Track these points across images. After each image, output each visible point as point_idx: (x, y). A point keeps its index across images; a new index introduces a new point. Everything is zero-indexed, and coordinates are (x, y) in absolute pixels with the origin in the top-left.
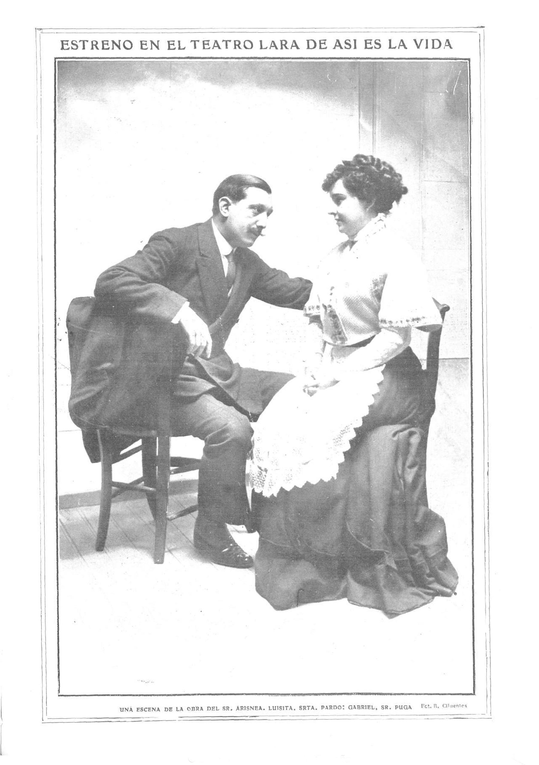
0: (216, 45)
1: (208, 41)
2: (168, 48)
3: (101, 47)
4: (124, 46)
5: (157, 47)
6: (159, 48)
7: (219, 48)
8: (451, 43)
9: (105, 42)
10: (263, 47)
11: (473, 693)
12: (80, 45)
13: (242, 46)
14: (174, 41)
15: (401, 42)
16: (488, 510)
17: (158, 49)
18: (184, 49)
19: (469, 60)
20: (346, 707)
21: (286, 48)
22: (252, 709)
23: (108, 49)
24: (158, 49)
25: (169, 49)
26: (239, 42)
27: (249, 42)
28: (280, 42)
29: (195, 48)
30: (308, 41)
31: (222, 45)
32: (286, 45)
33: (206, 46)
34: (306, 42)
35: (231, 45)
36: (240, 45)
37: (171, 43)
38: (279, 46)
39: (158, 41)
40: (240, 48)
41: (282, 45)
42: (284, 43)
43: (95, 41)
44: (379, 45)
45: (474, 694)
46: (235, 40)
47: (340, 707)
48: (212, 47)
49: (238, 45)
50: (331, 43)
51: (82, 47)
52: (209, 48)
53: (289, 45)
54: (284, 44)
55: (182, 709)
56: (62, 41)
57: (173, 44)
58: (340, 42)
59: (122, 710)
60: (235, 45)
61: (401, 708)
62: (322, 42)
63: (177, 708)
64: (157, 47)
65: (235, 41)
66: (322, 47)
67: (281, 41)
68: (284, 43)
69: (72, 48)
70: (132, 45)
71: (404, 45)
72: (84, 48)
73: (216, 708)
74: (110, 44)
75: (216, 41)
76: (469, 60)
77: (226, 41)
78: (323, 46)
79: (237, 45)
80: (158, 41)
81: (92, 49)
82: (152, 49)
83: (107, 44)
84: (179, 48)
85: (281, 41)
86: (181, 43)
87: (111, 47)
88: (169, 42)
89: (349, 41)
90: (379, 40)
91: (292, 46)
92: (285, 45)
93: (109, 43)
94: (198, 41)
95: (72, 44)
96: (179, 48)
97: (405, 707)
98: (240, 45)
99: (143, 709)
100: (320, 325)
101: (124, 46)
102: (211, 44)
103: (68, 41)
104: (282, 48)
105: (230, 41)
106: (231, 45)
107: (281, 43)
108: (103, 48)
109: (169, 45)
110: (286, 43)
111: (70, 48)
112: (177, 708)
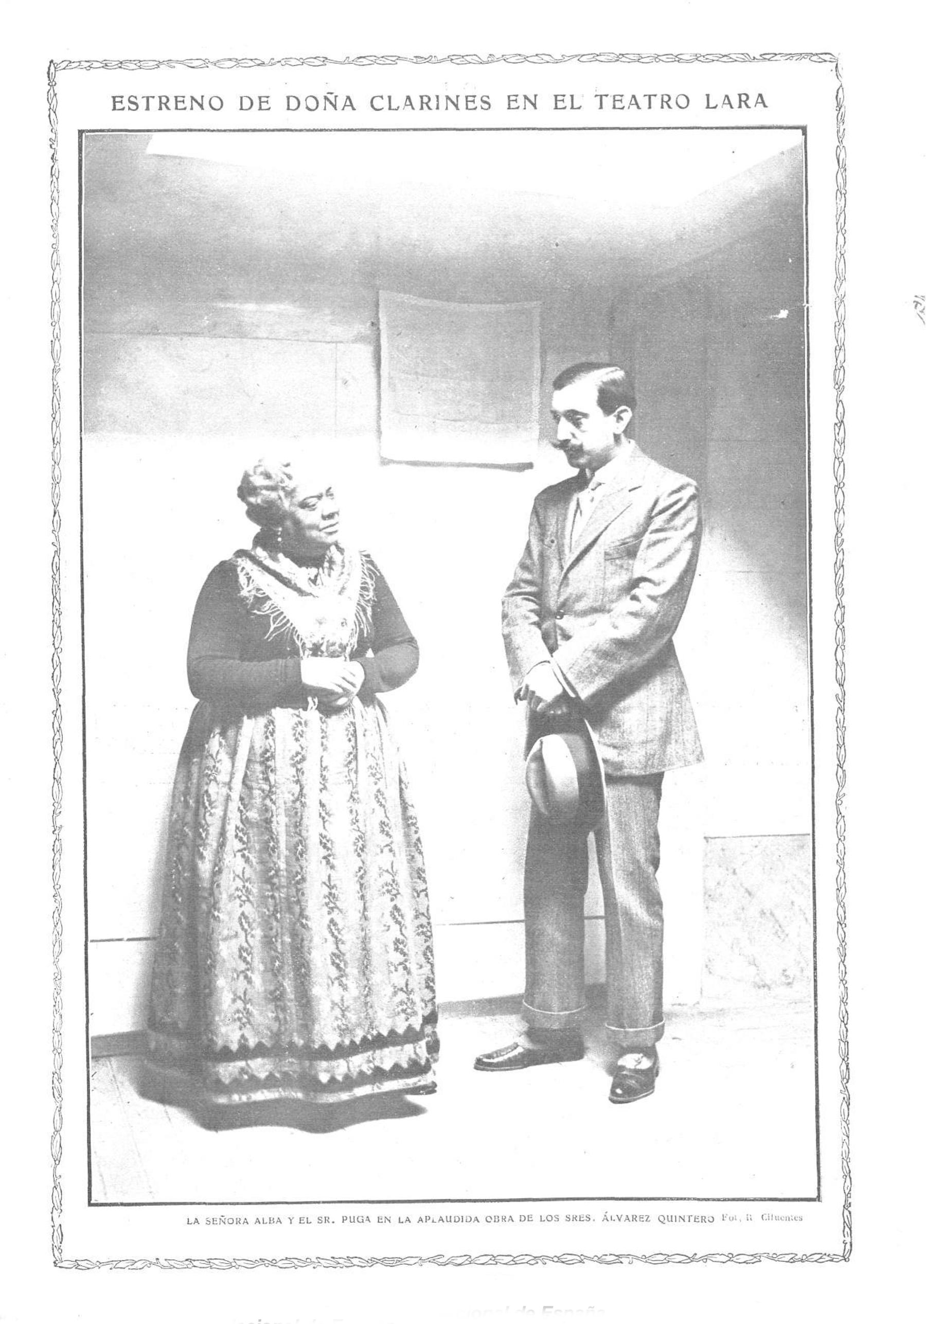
1: (622, 96)
2: (554, 106)
3: (174, 106)
5: (534, 105)
8: (765, 99)
10: (711, 106)
11: (92, 1202)
12: (142, 103)
13: (672, 103)
15: (348, 101)
17: (203, 109)
18: (579, 108)
19: (81, 132)
20: (536, 1218)
21: (747, 106)
22: (222, 1223)
24: (536, 108)
25: (556, 108)
28: (738, 97)
29: (601, 107)
30: (288, 98)
31: (643, 102)
32: (669, 103)
33: (618, 104)
34: (286, 99)
38: (631, 1219)
39: (535, 96)
40: (168, 108)
42: (744, 97)
43: (166, 97)
44: (487, 103)
45: (90, 1204)
46: (288, 94)
47: (549, 1218)
50: (277, 102)
51: (145, 107)
54: (743, 100)
55: (197, 1221)
57: (473, 101)
59: (670, 1219)
61: (352, 1220)
62: (263, 102)
63: (708, 96)
64: (534, 105)
67: (740, 95)
68: (425, 100)
69: (129, 109)
71: (763, 102)
72: (148, 109)
73: (305, 1220)
74: (521, 100)
75: (634, 97)
76: (81, 132)
77: (601, 96)
78: (264, 106)
79: (666, 102)
80: (535, 96)
81: (161, 109)
82: (192, 109)
84: (572, 108)
86: (574, 97)
88: (114, 98)
89: (136, 97)
90: (488, 97)
91: (757, 103)
93: (185, 99)
94: (655, 95)
95: (130, 102)
96: (572, 108)
97: (360, 1220)
99: (554, 1219)
102: (627, 100)
103: (122, 97)
104: (422, 108)
105: (607, 96)
106: (656, 102)
108: (176, 108)
109: (114, 102)
110: (748, 98)
111: (127, 108)
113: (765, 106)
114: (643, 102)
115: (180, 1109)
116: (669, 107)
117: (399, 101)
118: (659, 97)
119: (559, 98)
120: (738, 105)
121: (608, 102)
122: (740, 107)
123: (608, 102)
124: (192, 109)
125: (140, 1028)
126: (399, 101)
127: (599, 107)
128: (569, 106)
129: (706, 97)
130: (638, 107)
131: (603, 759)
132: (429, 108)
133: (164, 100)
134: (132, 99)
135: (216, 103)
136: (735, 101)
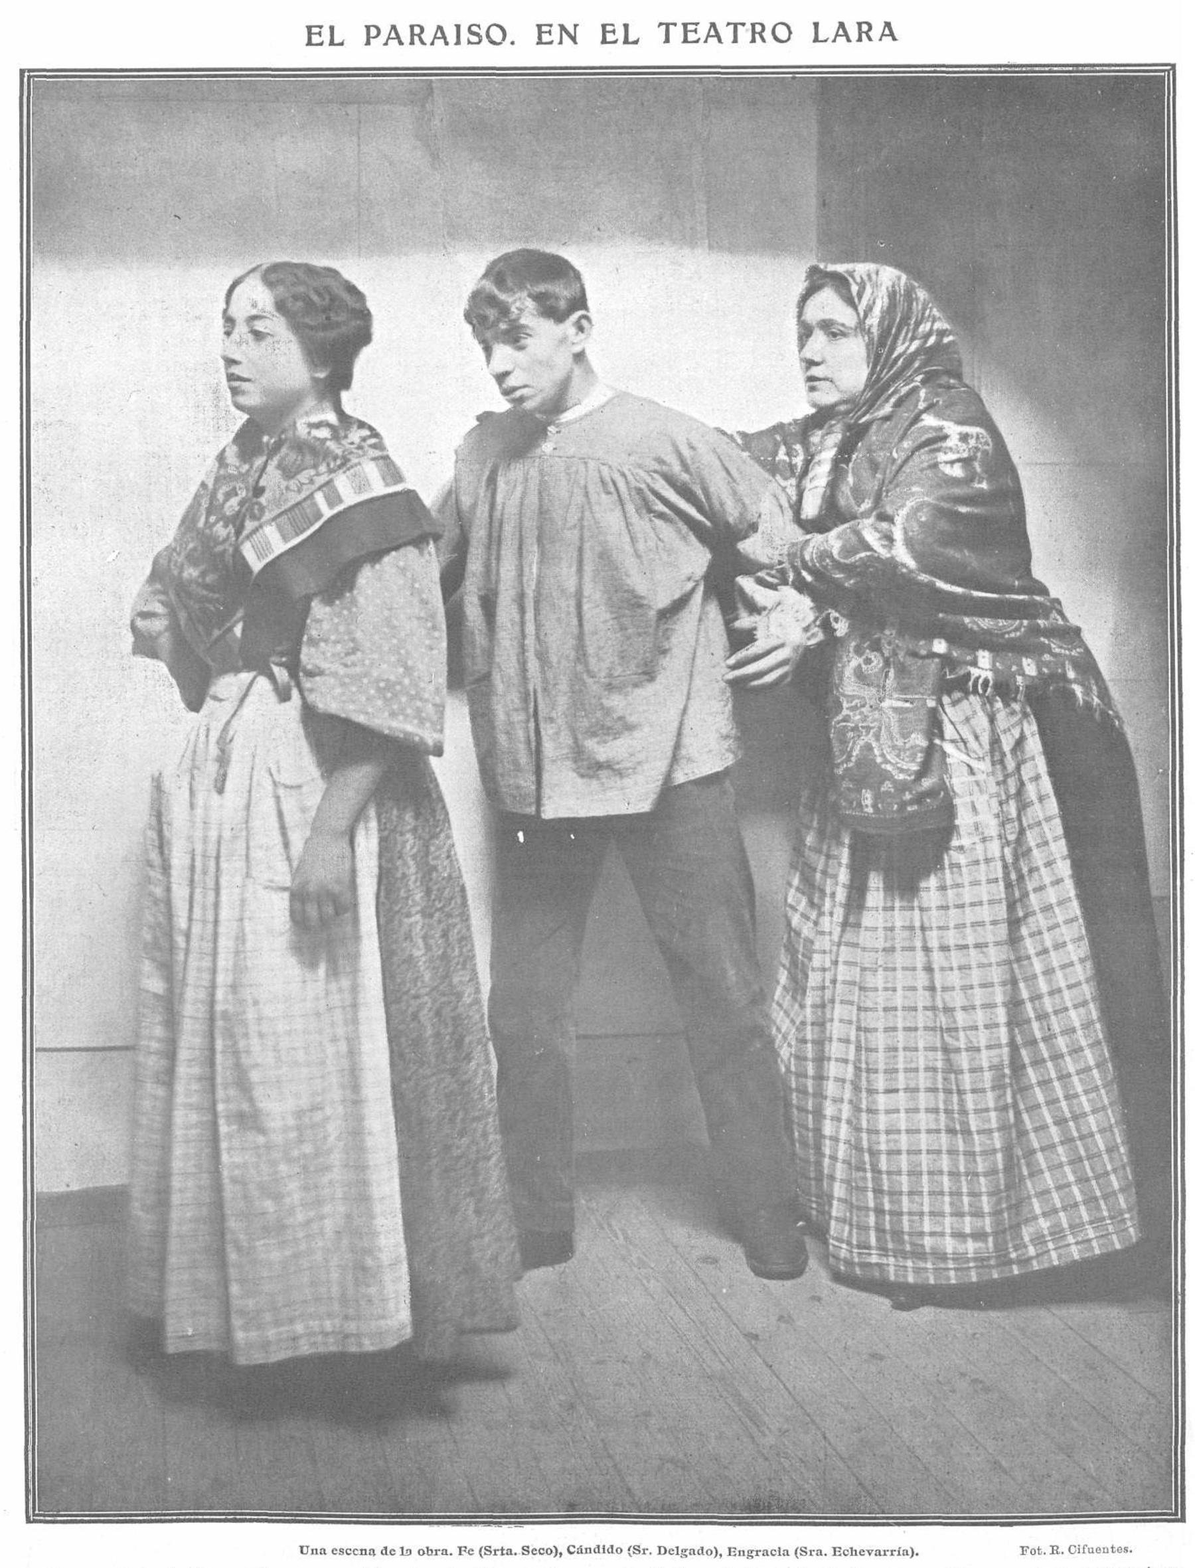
0: (712, 33)
1: (697, 24)
2: (306, 41)
4: (488, 36)
5: (574, 39)
6: (578, 40)
7: (720, 41)
9: (544, 29)
13: (767, 34)
14: (551, 26)
16: (853, 1552)
17: (575, 43)
19: (22, 72)
23: (551, 43)
24: (575, 43)
26: (763, 26)
27: (498, 30)
29: (667, 40)
31: (726, 33)
35: (744, 34)
36: (870, 33)
37: (544, 29)
38: (853, 34)
39: (576, 26)
41: (412, 34)
46: (860, 20)
48: (703, 39)
49: (760, 34)
52: (697, 41)
53: (428, 36)
56: (539, 26)
58: (445, 30)
60: (754, 32)
63: (816, 25)
64: (574, 39)
65: (753, 25)
66: (690, 39)
67: (412, 27)
70: (790, 33)
71: (892, 34)
73: (326, 33)
74: (556, 30)
75: (713, 25)
77: (736, 25)
79: (757, 32)
80: (576, 26)
81: (753, 41)
82: (561, 43)
83: (614, 32)
84: (332, 43)
85: (860, 24)
87: (557, 40)
91: (883, 35)
92: (867, 33)
98: (870, 33)
100: (489, 761)
101: (488, 36)
102: (703, 30)
103: (321, 27)
104: (412, 43)
106: (744, 34)
107: (860, 29)
110: (870, 28)
112: (816, 25)
113: (894, 39)
114: (726, 33)
115: (727, 644)
116: (764, 40)
117: (828, 30)
118: (749, 26)
119: (690, 27)
120: (857, 37)
121: (676, 33)
122: (412, 43)
123: (676, 33)
124: (561, 43)
125: (465, 697)
126: (828, 30)
127: (663, 38)
128: (621, 39)
129: (455, 29)
130: (720, 41)
131: (194, 704)
132: (870, 39)
133: (758, 29)
134: (474, 29)
135: (782, 32)
136: (405, 35)
